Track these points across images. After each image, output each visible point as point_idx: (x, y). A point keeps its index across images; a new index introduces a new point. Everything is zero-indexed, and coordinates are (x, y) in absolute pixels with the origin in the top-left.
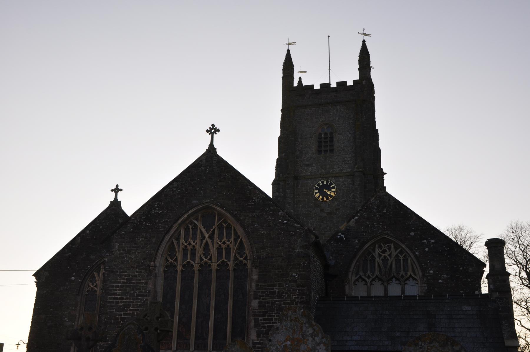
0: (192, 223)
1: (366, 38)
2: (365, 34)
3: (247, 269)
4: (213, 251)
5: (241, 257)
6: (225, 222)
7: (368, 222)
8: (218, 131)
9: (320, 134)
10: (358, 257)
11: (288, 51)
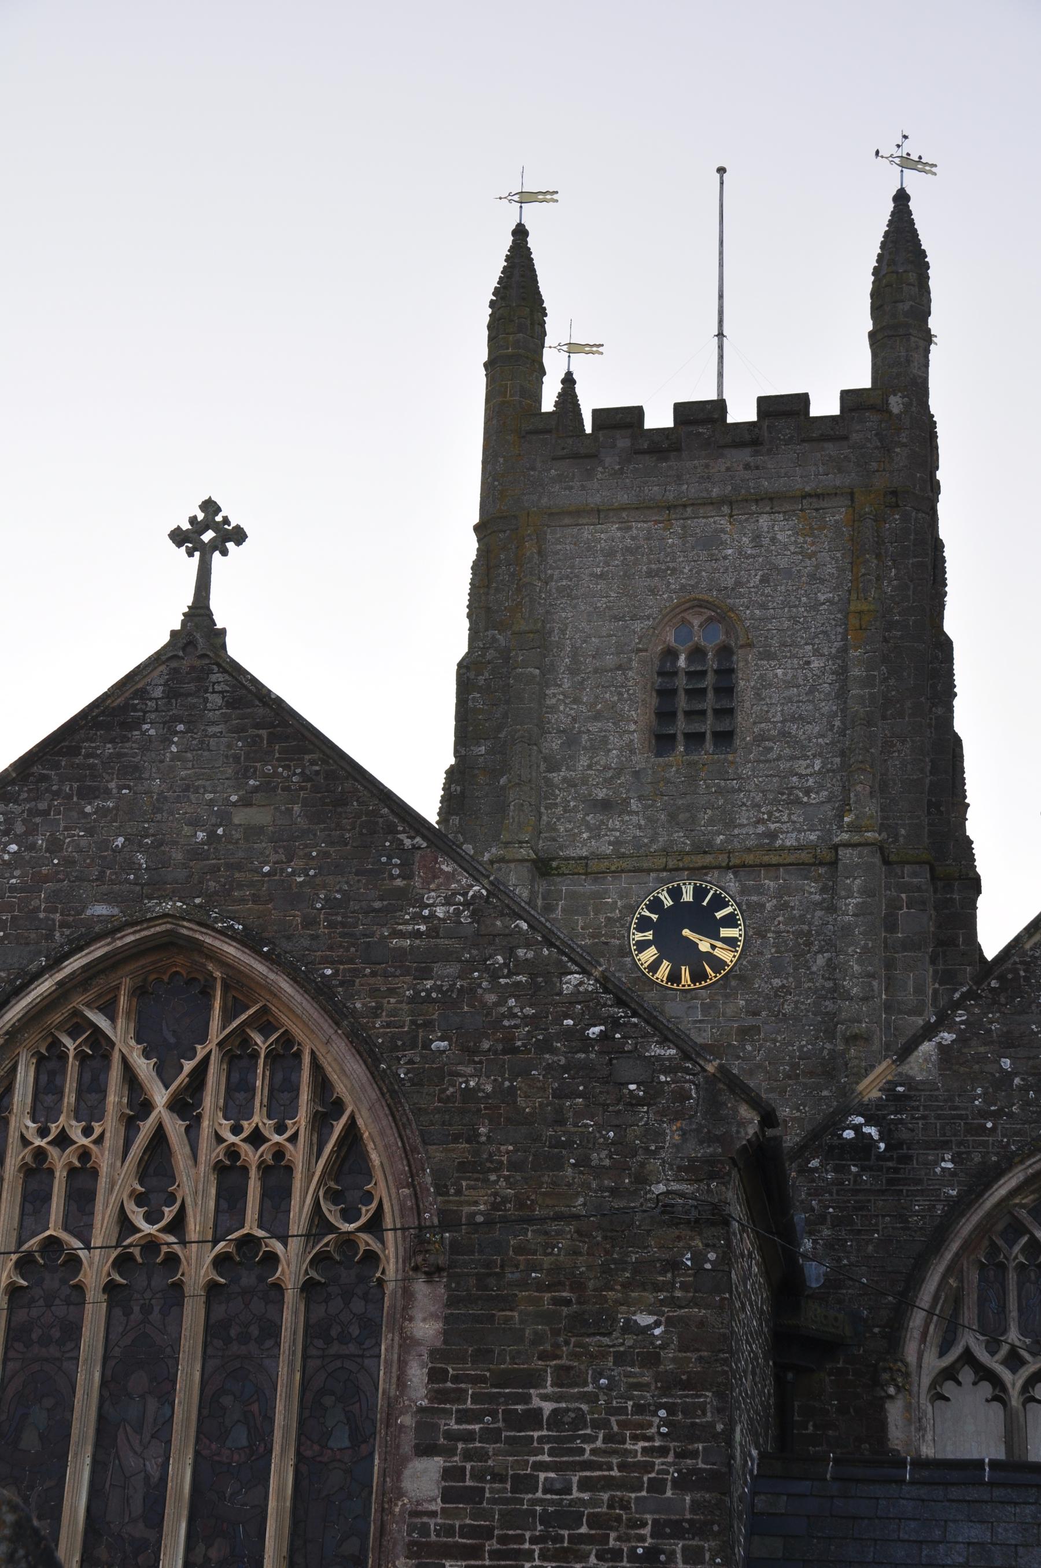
0: (78, 1025)
1: (914, 183)
2: (907, 163)
3: (381, 1282)
4: (195, 1186)
5: (349, 1215)
6: (265, 1023)
7: (1006, 1063)
8: (239, 536)
9: (671, 654)
10: (955, 1246)
11: (520, 233)
